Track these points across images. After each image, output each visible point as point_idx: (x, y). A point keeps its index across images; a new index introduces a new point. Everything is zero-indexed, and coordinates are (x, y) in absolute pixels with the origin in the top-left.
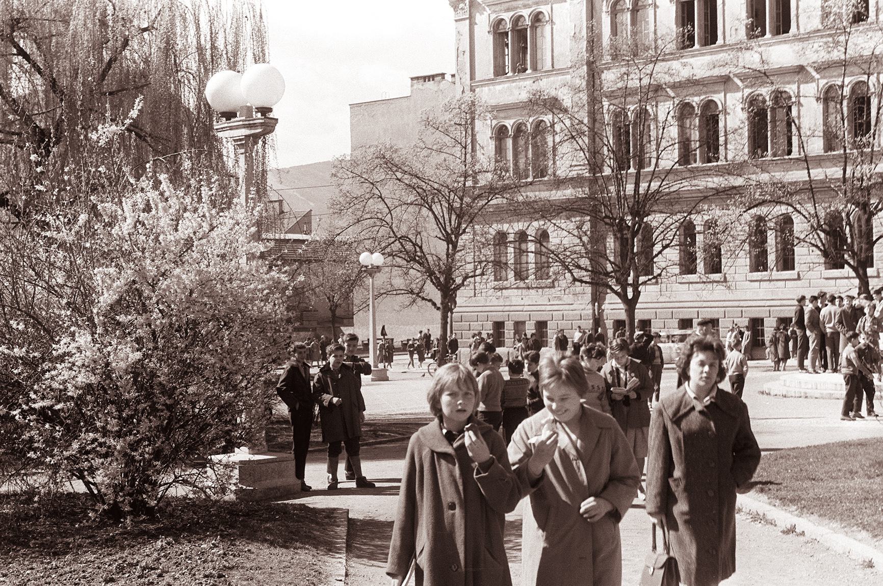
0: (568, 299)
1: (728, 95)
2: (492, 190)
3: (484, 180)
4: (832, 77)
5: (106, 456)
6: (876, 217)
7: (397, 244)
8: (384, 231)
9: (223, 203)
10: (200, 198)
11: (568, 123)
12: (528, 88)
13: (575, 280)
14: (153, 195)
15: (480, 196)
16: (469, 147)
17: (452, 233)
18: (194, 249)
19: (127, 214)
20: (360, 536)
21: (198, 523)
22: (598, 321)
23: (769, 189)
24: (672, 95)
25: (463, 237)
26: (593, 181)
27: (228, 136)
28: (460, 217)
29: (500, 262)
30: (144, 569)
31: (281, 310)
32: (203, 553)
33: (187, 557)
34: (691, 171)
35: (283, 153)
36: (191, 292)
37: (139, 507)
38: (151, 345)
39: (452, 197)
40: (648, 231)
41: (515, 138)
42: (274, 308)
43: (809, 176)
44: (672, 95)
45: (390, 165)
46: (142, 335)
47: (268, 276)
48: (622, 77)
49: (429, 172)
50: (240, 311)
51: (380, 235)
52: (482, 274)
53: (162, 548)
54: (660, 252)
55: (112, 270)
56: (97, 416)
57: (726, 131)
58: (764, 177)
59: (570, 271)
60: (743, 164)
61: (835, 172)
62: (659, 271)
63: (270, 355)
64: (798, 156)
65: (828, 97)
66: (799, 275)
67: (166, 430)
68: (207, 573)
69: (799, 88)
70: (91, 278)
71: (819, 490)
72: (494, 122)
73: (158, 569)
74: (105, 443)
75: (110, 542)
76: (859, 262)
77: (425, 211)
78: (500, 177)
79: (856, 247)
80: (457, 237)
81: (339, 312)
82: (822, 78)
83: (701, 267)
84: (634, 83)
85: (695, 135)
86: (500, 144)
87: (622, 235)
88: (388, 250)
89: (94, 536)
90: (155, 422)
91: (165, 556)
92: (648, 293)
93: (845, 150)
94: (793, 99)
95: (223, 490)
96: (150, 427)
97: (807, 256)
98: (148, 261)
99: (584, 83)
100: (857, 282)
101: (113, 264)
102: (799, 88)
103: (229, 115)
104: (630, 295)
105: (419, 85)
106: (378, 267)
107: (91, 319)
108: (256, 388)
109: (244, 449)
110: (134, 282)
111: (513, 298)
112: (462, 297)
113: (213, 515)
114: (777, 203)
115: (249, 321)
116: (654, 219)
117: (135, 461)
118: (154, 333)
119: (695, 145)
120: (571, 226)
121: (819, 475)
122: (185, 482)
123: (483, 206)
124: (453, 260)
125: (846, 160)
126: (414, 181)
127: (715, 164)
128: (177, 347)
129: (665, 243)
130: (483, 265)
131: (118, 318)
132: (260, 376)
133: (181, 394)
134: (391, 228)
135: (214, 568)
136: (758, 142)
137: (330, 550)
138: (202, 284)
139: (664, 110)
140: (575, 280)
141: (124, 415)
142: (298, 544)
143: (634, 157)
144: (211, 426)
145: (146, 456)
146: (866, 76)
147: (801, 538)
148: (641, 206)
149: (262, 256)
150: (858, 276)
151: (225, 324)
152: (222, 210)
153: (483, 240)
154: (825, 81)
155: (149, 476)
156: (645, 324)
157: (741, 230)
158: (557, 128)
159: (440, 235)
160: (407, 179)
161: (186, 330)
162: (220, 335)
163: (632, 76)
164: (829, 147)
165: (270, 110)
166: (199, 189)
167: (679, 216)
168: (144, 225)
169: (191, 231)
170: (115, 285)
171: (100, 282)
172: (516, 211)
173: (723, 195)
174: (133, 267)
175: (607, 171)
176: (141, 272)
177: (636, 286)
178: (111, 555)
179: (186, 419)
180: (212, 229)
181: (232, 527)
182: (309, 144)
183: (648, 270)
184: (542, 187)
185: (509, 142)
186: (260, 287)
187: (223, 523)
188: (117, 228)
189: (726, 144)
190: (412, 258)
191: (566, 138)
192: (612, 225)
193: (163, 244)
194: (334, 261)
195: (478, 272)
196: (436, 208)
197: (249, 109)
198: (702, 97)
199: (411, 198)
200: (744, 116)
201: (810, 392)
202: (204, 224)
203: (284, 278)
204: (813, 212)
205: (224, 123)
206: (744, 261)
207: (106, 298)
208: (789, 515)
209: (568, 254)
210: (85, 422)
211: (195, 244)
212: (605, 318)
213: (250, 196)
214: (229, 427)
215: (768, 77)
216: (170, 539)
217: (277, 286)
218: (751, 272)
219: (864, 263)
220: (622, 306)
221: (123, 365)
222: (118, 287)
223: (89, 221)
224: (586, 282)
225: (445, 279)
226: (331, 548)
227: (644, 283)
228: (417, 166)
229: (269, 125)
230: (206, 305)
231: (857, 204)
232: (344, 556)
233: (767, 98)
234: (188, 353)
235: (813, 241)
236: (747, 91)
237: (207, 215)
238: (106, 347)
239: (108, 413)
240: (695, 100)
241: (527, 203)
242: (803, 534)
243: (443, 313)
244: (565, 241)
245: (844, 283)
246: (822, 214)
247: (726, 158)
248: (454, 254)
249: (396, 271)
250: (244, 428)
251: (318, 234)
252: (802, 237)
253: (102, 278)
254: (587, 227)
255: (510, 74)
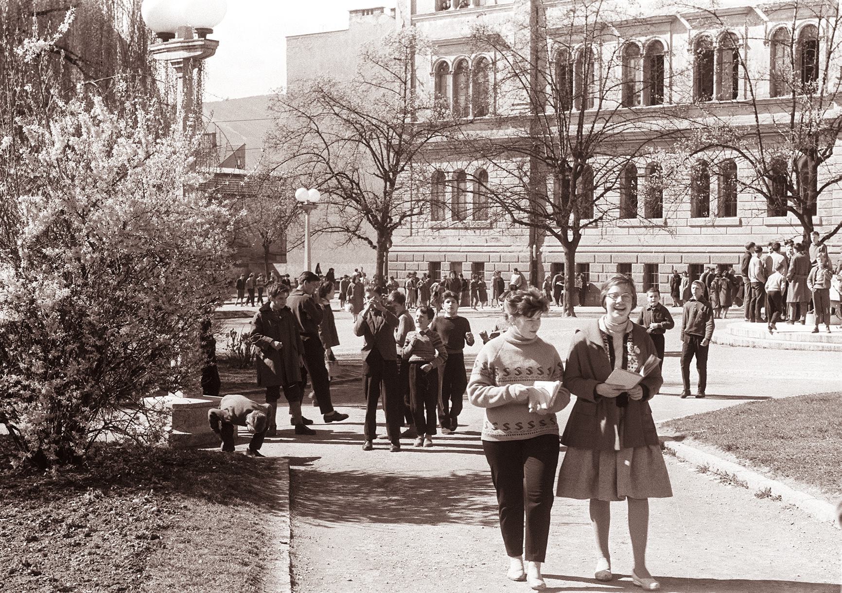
0: (506, 240)
1: (674, 36)
2: (432, 128)
3: (423, 117)
4: (782, 19)
5: (30, 400)
6: (824, 163)
7: (334, 180)
8: (320, 167)
9: (161, 128)
10: (136, 122)
11: (511, 59)
12: (471, 23)
13: (515, 221)
14: (84, 117)
15: (419, 133)
16: (409, 82)
17: (391, 170)
18: (128, 177)
19: (55, 138)
20: (304, 490)
21: (129, 474)
22: (535, 264)
23: (716, 133)
24: (618, 34)
25: (403, 174)
26: (535, 121)
27: (164, 60)
28: (398, 154)
29: (438, 201)
30: (70, 527)
31: (222, 248)
32: (134, 509)
33: (117, 514)
34: (635, 112)
35: (219, 81)
36: (125, 224)
37: (65, 456)
38: (80, 282)
39: (390, 134)
40: (587, 173)
41: (456, 75)
42: (214, 244)
43: (757, 121)
44: (618, 34)
45: (327, 99)
46: (71, 269)
47: (207, 209)
48: (567, 15)
49: (368, 107)
50: (177, 247)
51: (316, 170)
52: (421, 213)
53: (91, 503)
54: (602, 195)
55: (38, 199)
56: (21, 357)
57: (671, 72)
58: (710, 120)
59: (510, 212)
60: (688, 108)
61: (783, 117)
62: (601, 214)
63: (209, 294)
64: (743, 100)
65: (775, 40)
66: (741, 222)
67: (96, 373)
68: (140, 533)
69: (747, 30)
70: (16, 207)
71: (789, 449)
72: (435, 58)
73: (86, 527)
74: (29, 386)
75: (33, 494)
76: (805, 209)
77: (362, 147)
78: (440, 114)
79: (801, 194)
80: (394, 175)
81: (272, 248)
82: (771, 20)
83: (641, 210)
84: (579, 21)
85: (640, 76)
86: (440, 81)
87: (564, 176)
88: (325, 186)
89: (16, 486)
90: (84, 365)
91: (93, 512)
92: (589, 236)
93: (794, 95)
94: (741, 42)
95: (157, 436)
96: (78, 370)
97: (751, 202)
98: (78, 190)
99: (528, 21)
100: (801, 230)
101: (40, 192)
102: (747, 30)
103: (166, 36)
104: (570, 238)
105: (357, 18)
106: (314, 203)
107: (15, 252)
108: (194, 329)
109: (179, 393)
110: (62, 212)
111: (450, 238)
112: (397, 237)
113: (146, 464)
114: (724, 147)
115: (187, 258)
116: (597, 161)
117: (62, 406)
118: (83, 268)
119: (639, 86)
120: (512, 166)
121: (787, 431)
122: (116, 429)
123: (423, 144)
124: (390, 198)
125: (794, 105)
126: (353, 115)
127: (661, 106)
128: (109, 284)
129: (609, 185)
130: (421, 204)
131: (44, 250)
132: (197, 316)
133: (113, 335)
134: (328, 163)
135: (147, 528)
136: (703, 85)
137: (272, 507)
138: (137, 216)
139: (609, 50)
140: (515, 221)
141: (50, 356)
142: (238, 500)
143: (577, 97)
144: (144, 369)
145: (74, 401)
146: (817, 20)
147: (778, 503)
148: (584, 147)
149: (203, 188)
150: (804, 224)
151: (161, 260)
152: (157, 137)
153: (421, 178)
154: (774, 23)
155: (76, 422)
156: (584, 267)
157: (685, 175)
158: (500, 65)
159: (378, 172)
160: (345, 113)
161: (119, 265)
162: (156, 272)
163: (578, 13)
164: (775, 92)
165: (210, 31)
166: (134, 113)
167: (621, 159)
168: (73, 149)
169: (126, 158)
170: (41, 214)
171: (25, 211)
172: (456, 150)
173: (669, 138)
174: (61, 195)
175: (550, 111)
176: (70, 201)
177: (576, 229)
178: (34, 508)
179: (118, 361)
180: (148, 157)
181: (166, 479)
182: (244, 78)
183: (588, 214)
184: (483, 125)
185: (450, 79)
186: (199, 221)
187: (156, 474)
188: (44, 152)
189: (671, 85)
190: (348, 195)
191: (509, 75)
192: (554, 166)
193: (95, 172)
194: (268, 196)
195: (416, 211)
196: (374, 144)
197: (188, 30)
198: (648, 37)
199: (348, 134)
200: (692, 58)
201: (758, 342)
202: (140, 151)
203: (224, 211)
204: (758, 157)
205: (159, 44)
206: (687, 206)
207: (31, 230)
208: (762, 477)
209: (509, 194)
210: (8, 362)
211: (129, 172)
212: (543, 260)
213: (189, 123)
214: (164, 371)
215: (717, 18)
216: (99, 492)
217: (218, 221)
218: (692, 217)
219: (807, 213)
220: (562, 249)
221: (49, 302)
222: (45, 217)
223: (12, 145)
224: (526, 224)
225: (382, 218)
226: (273, 505)
227: (585, 226)
228: (355, 102)
229: (210, 49)
230: (140, 239)
231: (804, 150)
232: (287, 514)
233: (714, 39)
234: (121, 290)
235: (759, 188)
236: (694, 33)
237: (143, 141)
238: (31, 281)
239: (33, 354)
240: (641, 41)
241: (467, 142)
242: (779, 498)
243: (379, 252)
244: (505, 182)
245: (789, 229)
246: (768, 160)
247: (671, 100)
248: (392, 192)
249: (333, 208)
250: (180, 372)
251: (252, 168)
252: (748, 182)
253: (27, 207)
254: (527, 167)
255: (452, 9)
